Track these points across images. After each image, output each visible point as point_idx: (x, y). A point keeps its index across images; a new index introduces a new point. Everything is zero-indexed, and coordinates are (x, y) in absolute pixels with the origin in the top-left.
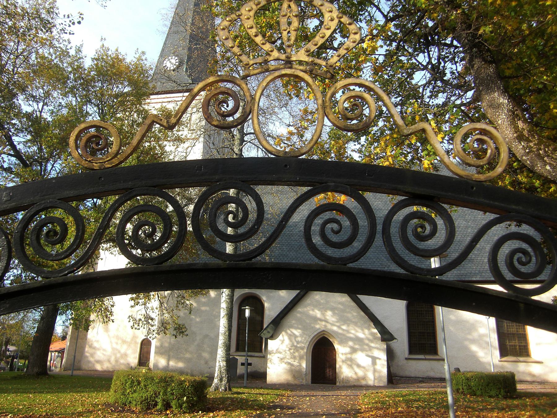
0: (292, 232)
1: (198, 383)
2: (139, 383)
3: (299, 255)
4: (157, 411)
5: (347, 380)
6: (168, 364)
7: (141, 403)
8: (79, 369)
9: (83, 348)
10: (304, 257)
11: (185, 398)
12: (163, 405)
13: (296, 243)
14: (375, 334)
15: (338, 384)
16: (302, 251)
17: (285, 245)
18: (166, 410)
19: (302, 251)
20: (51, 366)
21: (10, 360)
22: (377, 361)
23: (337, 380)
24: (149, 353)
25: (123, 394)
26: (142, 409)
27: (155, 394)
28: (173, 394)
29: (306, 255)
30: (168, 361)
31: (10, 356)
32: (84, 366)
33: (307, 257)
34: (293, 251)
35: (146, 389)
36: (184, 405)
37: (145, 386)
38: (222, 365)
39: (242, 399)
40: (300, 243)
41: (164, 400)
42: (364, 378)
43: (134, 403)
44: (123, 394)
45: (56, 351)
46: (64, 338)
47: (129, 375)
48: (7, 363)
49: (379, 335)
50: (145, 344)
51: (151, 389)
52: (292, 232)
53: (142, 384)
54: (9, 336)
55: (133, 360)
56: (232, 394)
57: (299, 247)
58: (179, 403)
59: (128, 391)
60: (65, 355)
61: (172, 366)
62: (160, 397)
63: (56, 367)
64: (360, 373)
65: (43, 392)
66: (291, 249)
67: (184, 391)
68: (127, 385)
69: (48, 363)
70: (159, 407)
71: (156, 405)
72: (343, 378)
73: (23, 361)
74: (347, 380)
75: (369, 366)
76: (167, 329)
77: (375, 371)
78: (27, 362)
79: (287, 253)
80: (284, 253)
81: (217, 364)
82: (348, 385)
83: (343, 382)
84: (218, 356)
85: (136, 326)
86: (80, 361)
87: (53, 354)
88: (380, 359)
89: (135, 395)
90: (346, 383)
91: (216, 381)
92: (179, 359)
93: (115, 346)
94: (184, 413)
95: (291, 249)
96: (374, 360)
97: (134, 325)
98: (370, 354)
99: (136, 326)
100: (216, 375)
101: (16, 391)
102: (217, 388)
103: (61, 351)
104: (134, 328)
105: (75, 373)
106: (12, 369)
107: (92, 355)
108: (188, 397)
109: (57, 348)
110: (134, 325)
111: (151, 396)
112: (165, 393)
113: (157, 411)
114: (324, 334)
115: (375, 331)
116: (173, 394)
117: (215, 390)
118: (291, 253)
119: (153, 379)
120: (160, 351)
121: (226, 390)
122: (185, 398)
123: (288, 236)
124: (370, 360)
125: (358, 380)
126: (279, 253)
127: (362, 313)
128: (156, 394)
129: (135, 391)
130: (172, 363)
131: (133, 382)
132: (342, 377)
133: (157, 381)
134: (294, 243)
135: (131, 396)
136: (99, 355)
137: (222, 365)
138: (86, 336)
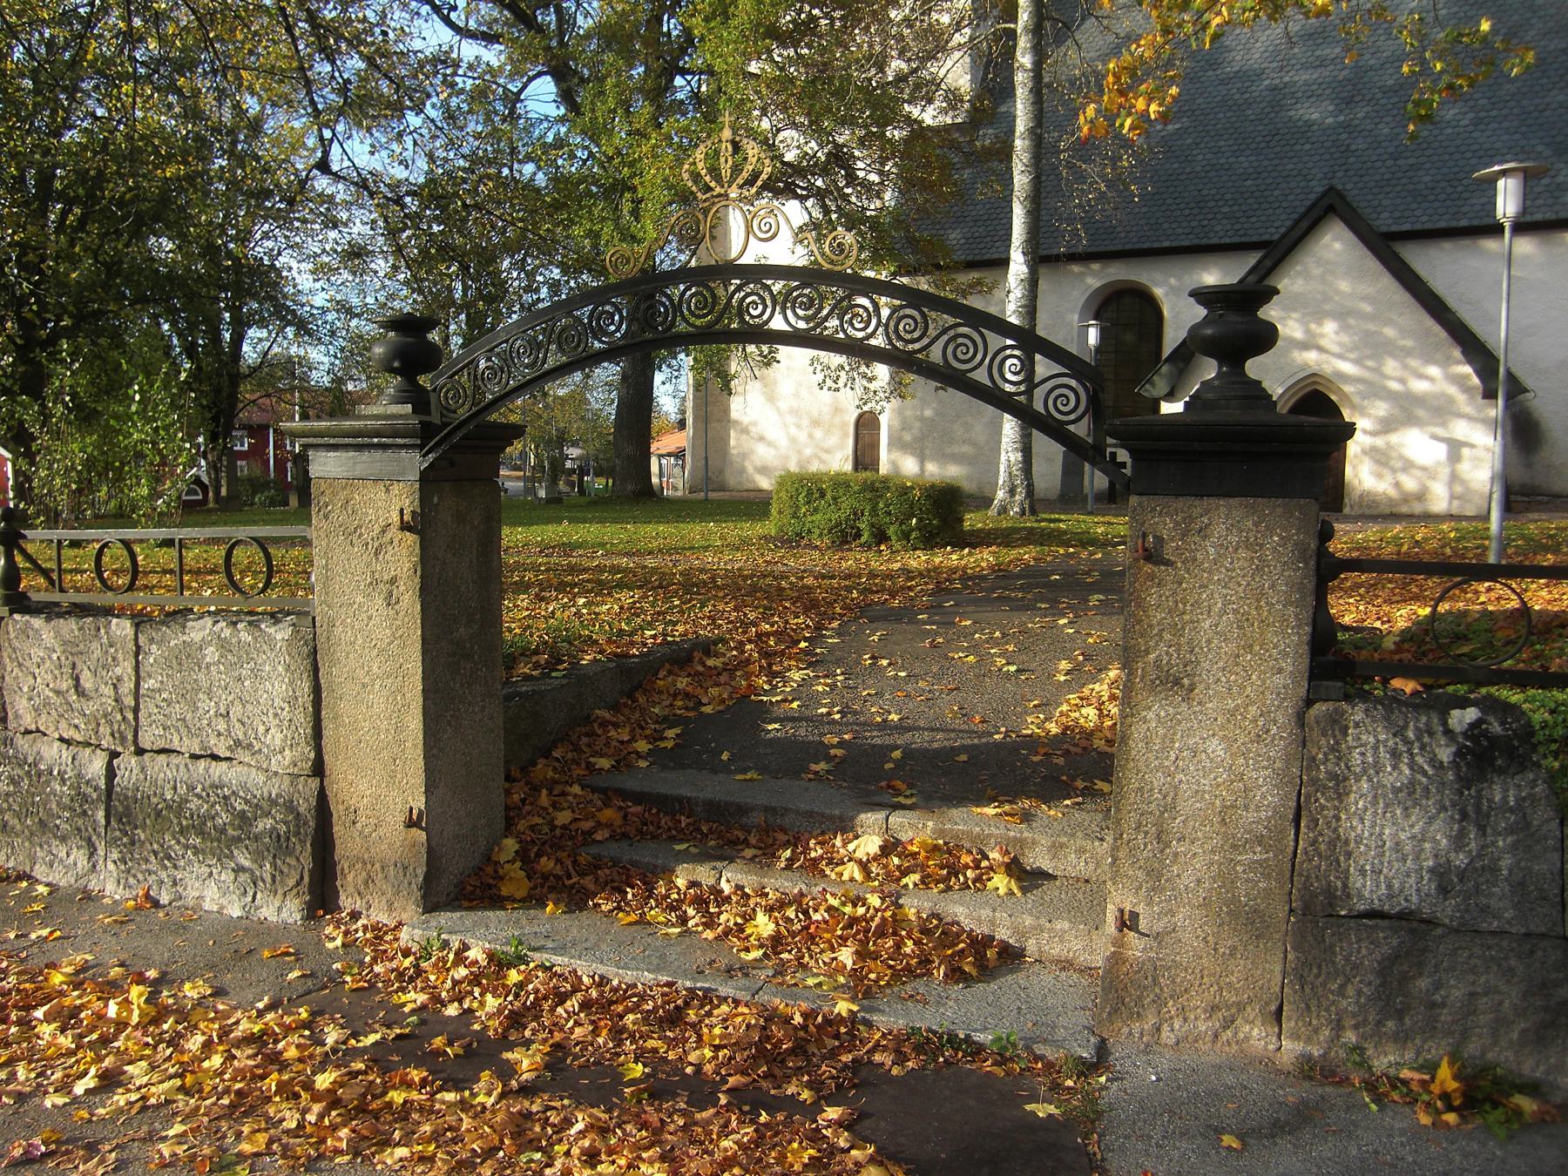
0: (1247, 95)
1: (939, 491)
2: (823, 495)
3: (1266, 163)
4: (861, 545)
5: (1373, 502)
6: (922, 470)
7: (830, 532)
8: (723, 488)
9: (725, 440)
10: (1280, 168)
11: (914, 521)
12: (872, 535)
13: (1261, 128)
14: (1467, 377)
15: (1347, 510)
16: (1276, 150)
17: (1225, 137)
18: (879, 544)
19: (1276, 150)
20: (665, 485)
21: (575, 478)
22: (1465, 451)
23: (1346, 501)
24: (875, 445)
25: (795, 516)
26: (833, 542)
27: (855, 514)
28: (889, 513)
29: (1286, 161)
30: (922, 463)
31: (573, 471)
32: (732, 481)
33: (1291, 166)
34: (1249, 152)
35: (836, 504)
36: (914, 535)
37: (834, 499)
38: (1012, 459)
39: (1058, 530)
40: (1271, 127)
41: (873, 525)
42: (1421, 496)
43: (817, 532)
44: (795, 516)
45: (669, 455)
46: (682, 424)
47: (801, 481)
48: (572, 484)
49: (1475, 380)
50: (866, 425)
51: (846, 504)
52: (1247, 95)
53: (828, 496)
54: (562, 425)
55: (840, 460)
56: (1037, 521)
57: (1268, 138)
58: (903, 531)
59: (803, 510)
60: (688, 459)
61: (932, 475)
62: (865, 518)
63: (675, 488)
64: (1410, 484)
65: (650, 522)
66: (1242, 147)
67: (912, 506)
68: (800, 498)
69: (655, 480)
70: (863, 539)
71: (858, 535)
72: (1361, 496)
73: (603, 481)
74: (1369, 501)
75: (1438, 463)
76: (905, 386)
77: (1454, 478)
78: (610, 481)
79: (1231, 160)
80: (1222, 161)
81: (1003, 458)
82: (1375, 512)
83: (1361, 506)
84: (1004, 440)
85: (829, 383)
86: (721, 471)
87: (664, 461)
88: (1472, 446)
89: (818, 517)
90: (1369, 507)
91: (1000, 494)
92: (944, 457)
93: (793, 431)
94: (915, 549)
95: (1242, 147)
96: (1455, 448)
97: (824, 381)
98: (1440, 432)
99: (829, 383)
100: (1001, 482)
101: (602, 521)
102: (1003, 510)
103: (679, 454)
104: (825, 388)
105: (712, 495)
106: (582, 491)
107: (744, 456)
108: (920, 520)
109: (672, 449)
110: (824, 381)
111: (847, 519)
112: (874, 510)
113: (861, 545)
114: (1315, 383)
115: (1467, 369)
116: (889, 513)
117: (999, 514)
118: (1242, 159)
119: (849, 486)
120: (897, 443)
121: (1023, 513)
122: (914, 521)
123: (1235, 108)
124: (1441, 451)
125: (1407, 498)
126: (1205, 162)
127: (1430, 323)
128: (857, 515)
129: (816, 510)
130: (932, 468)
131: (810, 493)
132: (1358, 493)
133: (856, 488)
134: (1251, 129)
135: (810, 518)
136: (763, 454)
137: (1012, 459)
138: (727, 411)
